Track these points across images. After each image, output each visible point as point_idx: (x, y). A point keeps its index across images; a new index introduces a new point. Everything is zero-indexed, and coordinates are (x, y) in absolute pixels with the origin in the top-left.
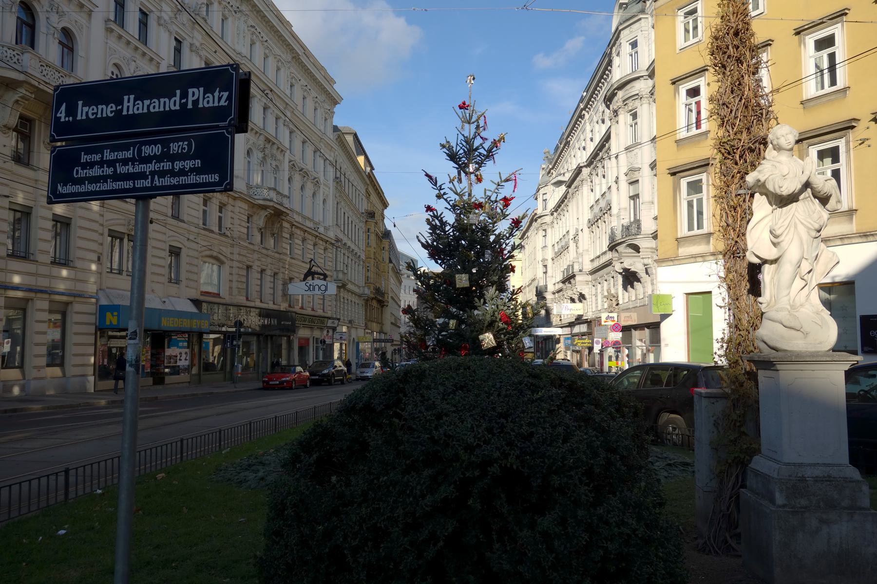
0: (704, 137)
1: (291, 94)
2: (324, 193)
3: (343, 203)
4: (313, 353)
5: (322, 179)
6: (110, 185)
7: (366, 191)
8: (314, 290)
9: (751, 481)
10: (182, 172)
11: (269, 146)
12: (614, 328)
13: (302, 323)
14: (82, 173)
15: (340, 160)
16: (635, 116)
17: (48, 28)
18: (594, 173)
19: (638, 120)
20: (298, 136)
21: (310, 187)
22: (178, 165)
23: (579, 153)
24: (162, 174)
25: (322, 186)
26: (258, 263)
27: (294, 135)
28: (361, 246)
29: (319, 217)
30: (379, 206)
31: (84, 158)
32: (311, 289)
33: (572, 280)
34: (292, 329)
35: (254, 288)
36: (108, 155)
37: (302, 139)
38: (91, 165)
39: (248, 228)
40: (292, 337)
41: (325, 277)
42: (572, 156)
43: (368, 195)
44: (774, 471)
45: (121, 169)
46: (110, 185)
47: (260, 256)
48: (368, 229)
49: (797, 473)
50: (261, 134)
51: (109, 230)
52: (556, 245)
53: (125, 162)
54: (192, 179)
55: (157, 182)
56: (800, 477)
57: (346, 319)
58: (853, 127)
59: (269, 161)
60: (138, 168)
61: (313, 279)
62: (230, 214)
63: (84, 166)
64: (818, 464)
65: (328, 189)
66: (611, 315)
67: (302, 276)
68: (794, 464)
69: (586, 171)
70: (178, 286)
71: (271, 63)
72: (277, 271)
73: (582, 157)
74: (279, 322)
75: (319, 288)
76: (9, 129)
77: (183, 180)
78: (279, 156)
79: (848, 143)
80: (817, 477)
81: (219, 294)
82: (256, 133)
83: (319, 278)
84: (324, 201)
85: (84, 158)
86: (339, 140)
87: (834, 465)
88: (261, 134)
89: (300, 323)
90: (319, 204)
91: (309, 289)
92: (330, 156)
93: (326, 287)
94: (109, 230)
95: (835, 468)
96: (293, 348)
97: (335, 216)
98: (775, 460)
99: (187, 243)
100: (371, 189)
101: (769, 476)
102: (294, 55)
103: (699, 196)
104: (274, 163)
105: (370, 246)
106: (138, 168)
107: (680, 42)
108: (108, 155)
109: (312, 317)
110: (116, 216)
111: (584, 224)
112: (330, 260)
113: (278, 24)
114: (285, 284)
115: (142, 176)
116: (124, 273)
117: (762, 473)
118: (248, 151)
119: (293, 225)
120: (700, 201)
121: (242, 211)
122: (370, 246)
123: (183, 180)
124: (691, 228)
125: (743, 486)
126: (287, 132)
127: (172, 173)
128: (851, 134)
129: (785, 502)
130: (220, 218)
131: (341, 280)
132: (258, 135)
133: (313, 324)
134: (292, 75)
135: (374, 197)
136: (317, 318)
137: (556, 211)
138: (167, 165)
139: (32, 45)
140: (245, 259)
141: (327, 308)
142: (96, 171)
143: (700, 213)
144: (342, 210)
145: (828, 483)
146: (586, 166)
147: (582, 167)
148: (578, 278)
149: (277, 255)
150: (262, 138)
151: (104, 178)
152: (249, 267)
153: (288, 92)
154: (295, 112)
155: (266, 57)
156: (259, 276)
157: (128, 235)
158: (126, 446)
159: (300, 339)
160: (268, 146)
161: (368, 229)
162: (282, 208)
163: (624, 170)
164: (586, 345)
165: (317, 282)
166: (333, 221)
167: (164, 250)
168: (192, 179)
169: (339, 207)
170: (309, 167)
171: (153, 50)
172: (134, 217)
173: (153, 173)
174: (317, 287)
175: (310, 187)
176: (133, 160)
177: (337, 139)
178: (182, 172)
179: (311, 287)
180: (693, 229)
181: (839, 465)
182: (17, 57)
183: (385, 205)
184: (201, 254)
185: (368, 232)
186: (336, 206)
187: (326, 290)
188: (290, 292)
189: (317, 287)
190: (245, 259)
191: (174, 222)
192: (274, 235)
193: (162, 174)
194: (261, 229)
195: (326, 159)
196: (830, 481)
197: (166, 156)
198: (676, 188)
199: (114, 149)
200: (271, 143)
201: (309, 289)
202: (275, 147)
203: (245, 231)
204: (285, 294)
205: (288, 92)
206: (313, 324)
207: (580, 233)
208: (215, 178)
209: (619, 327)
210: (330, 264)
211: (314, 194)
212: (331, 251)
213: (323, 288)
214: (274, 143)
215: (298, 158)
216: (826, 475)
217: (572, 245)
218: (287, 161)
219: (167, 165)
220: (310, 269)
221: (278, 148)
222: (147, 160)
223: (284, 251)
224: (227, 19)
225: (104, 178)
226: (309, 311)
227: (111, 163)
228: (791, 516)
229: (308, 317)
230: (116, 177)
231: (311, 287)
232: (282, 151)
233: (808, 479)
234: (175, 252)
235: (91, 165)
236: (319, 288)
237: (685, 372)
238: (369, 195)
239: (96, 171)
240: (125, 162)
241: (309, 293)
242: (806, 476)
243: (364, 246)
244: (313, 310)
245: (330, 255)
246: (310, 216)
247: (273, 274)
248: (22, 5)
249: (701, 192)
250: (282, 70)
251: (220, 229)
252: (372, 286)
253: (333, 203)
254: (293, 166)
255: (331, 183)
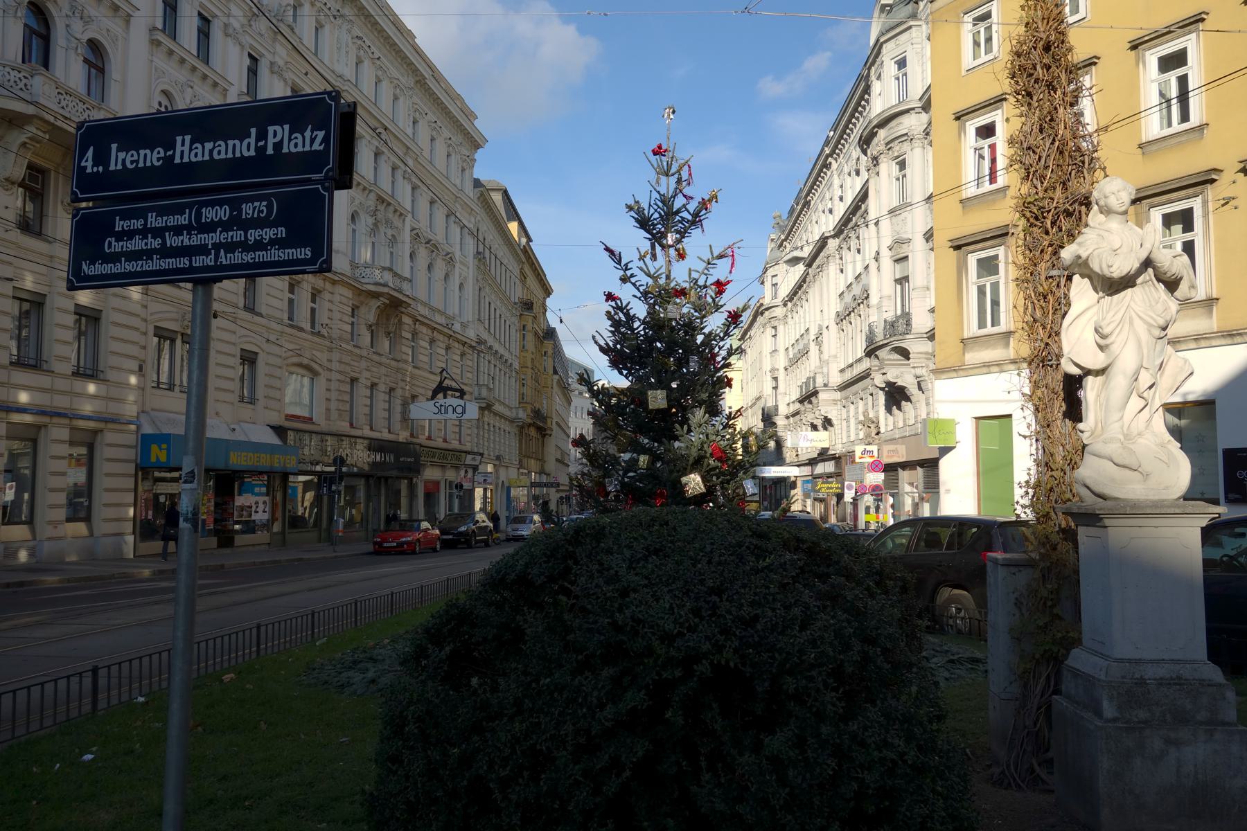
0: (1001, 195)
1: (414, 134)
2: (460, 274)
3: (487, 289)
4: (446, 503)
5: (458, 254)
6: (156, 264)
7: (521, 272)
8: (446, 412)
9: (1068, 684)
10: (259, 245)
11: (383, 207)
12: (874, 466)
13: (429, 459)
14: (117, 246)
15: (483, 228)
16: (902, 165)
17: (68, 40)
18: (844, 246)
19: (908, 171)
20: (424, 194)
21: (440, 266)
22: (253, 235)
23: (823, 218)
24: (230, 247)
25: (458, 265)
26: (367, 374)
27: (418, 192)
28: (513, 350)
29: (453, 309)
30: (539, 292)
31: (120, 225)
32: (443, 412)
33: (813, 399)
34: (416, 469)
35: (361, 410)
36: (154, 221)
37: (429, 198)
38: (130, 234)
39: (353, 324)
40: (415, 480)
41: (462, 394)
42: (814, 222)
43: (524, 277)
44: (1101, 670)
45: (172, 241)
46: (156, 264)
47: (369, 364)
48: (524, 326)
49: (1134, 673)
50: (371, 191)
51: (156, 327)
52: (790, 349)
53: (178, 230)
54: (273, 255)
55: (224, 259)
56: (1137, 679)
57: (492, 454)
58: (1213, 181)
59: (382, 229)
60: (197, 239)
61: (445, 397)
62: (327, 305)
63: (120, 236)
64: (1163, 660)
65: (466, 269)
66: (869, 448)
67: (430, 393)
68: (1129, 661)
69: (833, 244)
70: (252, 407)
71: (386, 89)
72: (394, 385)
73: (828, 224)
74: (397, 459)
75: (454, 410)
76: (13, 183)
77: (260, 256)
78: (397, 222)
79: (1205, 203)
80: (1161, 679)
81: (311, 419)
82: (365, 189)
83: (453, 396)
84: (461, 285)
85: (120, 225)
86: (481, 199)
87: (1185, 662)
88: (371, 191)
89: (426, 459)
90: (453, 291)
91: (440, 411)
92: (470, 222)
93: (464, 409)
94: (156, 327)
95: (1188, 666)
96: (417, 496)
97: (477, 307)
98: (1102, 654)
99: (265, 346)
100: (527, 269)
101: (1093, 677)
102: (418, 79)
103: (993, 278)
104: (390, 232)
105: (527, 351)
106: (197, 239)
107: (967, 60)
108: (154, 221)
109: (443, 452)
110: (165, 308)
111: (830, 319)
112: (470, 369)
113: (395, 34)
114: (405, 405)
115: (202, 250)
116: (177, 389)
117: (1084, 673)
118: (353, 215)
119: (417, 320)
120: (995, 286)
121: (344, 300)
122: (527, 351)
123: (260, 256)
124: (982, 324)
125: (1057, 691)
126: (408, 188)
127: (245, 247)
128: (1210, 191)
129: (1117, 715)
130: (313, 310)
131: (484, 399)
132: (367, 192)
133: (445, 461)
134: (416, 106)
135: (531, 281)
136: (451, 453)
137: (791, 300)
138: (237, 235)
139: (46, 65)
140: (348, 369)
141: (466, 439)
142: (137, 244)
143: (995, 303)
144: (487, 299)
145: (1178, 687)
146: (833, 237)
147: (827, 238)
148: (821, 396)
149: (393, 363)
150: (372, 196)
151: (147, 254)
152: (353, 380)
153: (409, 131)
154: (419, 160)
155: (378, 81)
156: (368, 392)
157: (182, 334)
158: (179, 634)
159: (426, 482)
160: (381, 208)
161: (524, 326)
162: (400, 297)
163: (887, 241)
164: (834, 490)
165: (451, 401)
166: (473, 314)
167: (234, 356)
168: (273, 255)
169: (483, 294)
170: (439, 237)
171: (218, 71)
172: (190, 309)
173: (217, 247)
174: (450, 409)
175: (440, 266)
176: (189, 228)
177: (479, 198)
178: (259, 245)
179: (443, 408)
180: (985, 327)
181: (1193, 662)
182: (24, 81)
183: (548, 291)
184: (285, 362)
185: (524, 330)
186: (477, 293)
187: (463, 412)
188: (412, 416)
189: (450, 409)
190: (348, 369)
191: (248, 316)
192: (389, 334)
193: (230, 247)
194: (370, 326)
195: (463, 227)
196: (1180, 684)
197: (235, 222)
198: (962, 267)
199: (162, 212)
200: (385, 204)
201: (440, 411)
202: (391, 209)
203: (348, 328)
204: (405, 419)
205: (409, 131)
206: (445, 461)
207: (825, 331)
208: (306, 253)
209: (880, 466)
210: (469, 375)
211: (447, 277)
212: (471, 358)
213: (459, 410)
214: (389, 204)
215: (423, 224)
216: (1174, 676)
217: (813, 348)
218: (408, 229)
219: (237, 235)
220: (441, 383)
221: (396, 211)
222: (209, 228)
223: (404, 357)
224: (322, 26)
225: (147, 254)
226: (439, 443)
227: (158, 232)
228: (1124, 735)
229: (438, 451)
230: (165, 252)
231: (443, 408)
232: (401, 214)
233: (1148, 681)
234: (249, 359)
235: (130, 234)
236: (454, 410)
237: (975, 530)
238: (525, 278)
239: (137, 244)
240: (178, 230)
241: (439, 416)
242: (1146, 677)
243: (518, 350)
244: (445, 441)
245: (470, 363)
246: (441, 308)
247: (388, 391)
248: (31, 7)
249: (997, 273)
250: (402, 99)
251: (313, 326)
252: (529, 408)
253: (474, 290)
254: (416, 237)
255: (471, 260)
